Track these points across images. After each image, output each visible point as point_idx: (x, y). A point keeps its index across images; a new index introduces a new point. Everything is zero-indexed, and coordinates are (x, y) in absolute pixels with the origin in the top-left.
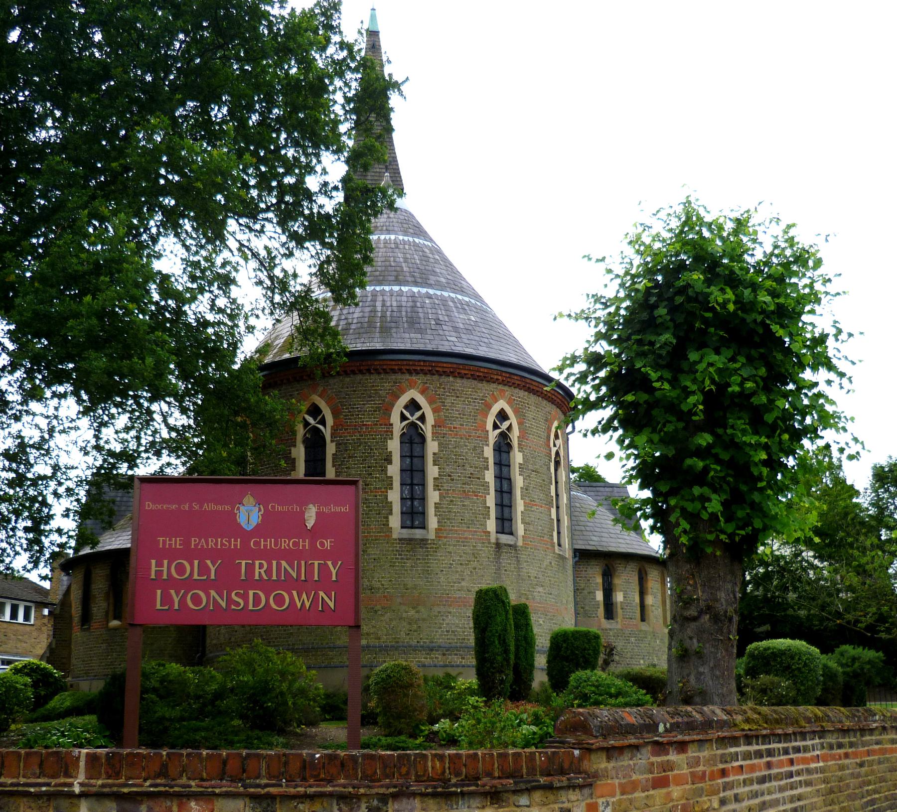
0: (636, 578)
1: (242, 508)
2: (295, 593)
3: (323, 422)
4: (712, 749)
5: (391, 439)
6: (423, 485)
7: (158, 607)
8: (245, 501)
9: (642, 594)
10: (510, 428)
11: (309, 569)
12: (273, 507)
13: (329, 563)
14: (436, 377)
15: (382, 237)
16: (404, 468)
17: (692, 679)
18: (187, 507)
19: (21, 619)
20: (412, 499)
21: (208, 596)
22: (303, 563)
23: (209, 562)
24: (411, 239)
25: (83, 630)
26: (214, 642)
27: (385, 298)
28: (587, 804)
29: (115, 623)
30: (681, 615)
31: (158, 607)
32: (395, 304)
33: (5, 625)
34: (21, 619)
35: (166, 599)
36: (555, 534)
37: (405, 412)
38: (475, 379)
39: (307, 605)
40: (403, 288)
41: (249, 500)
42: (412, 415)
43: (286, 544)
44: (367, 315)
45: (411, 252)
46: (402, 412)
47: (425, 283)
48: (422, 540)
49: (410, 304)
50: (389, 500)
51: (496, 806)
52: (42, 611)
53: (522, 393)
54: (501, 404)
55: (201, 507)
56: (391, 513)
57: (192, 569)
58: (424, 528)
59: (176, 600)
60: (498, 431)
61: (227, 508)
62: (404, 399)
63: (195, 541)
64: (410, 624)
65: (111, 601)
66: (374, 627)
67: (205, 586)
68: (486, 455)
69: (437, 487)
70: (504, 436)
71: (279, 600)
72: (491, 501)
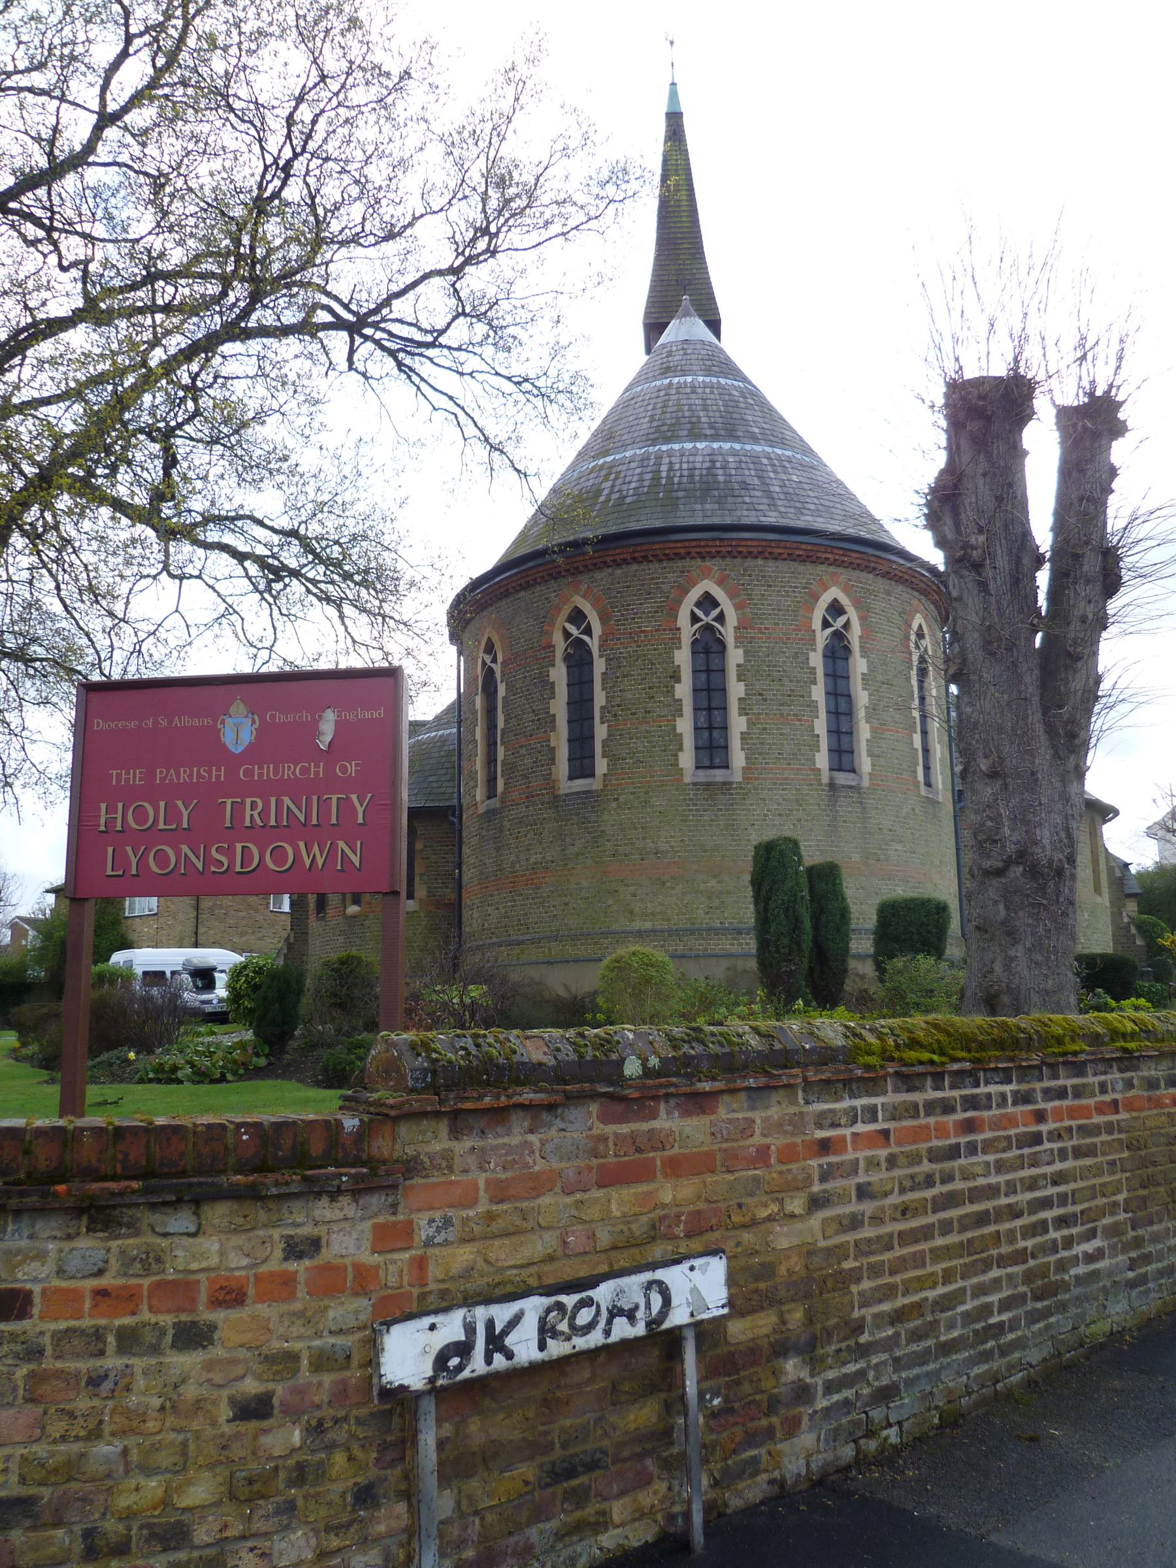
1: (228, 721)
3: (588, 631)
4: (794, 1102)
5: (679, 648)
6: (724, 709)
8: (232, 710)
10: (846, 626)
11: (324, 804)
12: (273, 717)
13: (354, 797)
14: (739, 560)
15: (676, 380)
16: (699, 686)
17: (998, 967)
18: (150, 723)
20: (710, 728)
21: (178, 853)
23: (180, 803)
24: (714, 380)
27: (674, 460)
28: (375, 1226)
29: (353, 909)
30: (980, 868)
31: (109, 872)
32: (685, 466)
35: (120, 859)
37: (697, 611)
39: (320, 861)
40: (698, 445)
41: (238, 708)
42: (707, 615)
43: (291, 771)
44: (646, 483)
46: (692, 613)
47: (732, 436)
48: (725, 783)
49: (707, 465)
50: (679, 730)
51: (101, 1235)
54: (834, 593)
55: (170, 723)
56: (681, 749)
58: (727, 767)
59: (134, 861)
60: (829, 630)
61: (207, 721)
62: (695, 594)
64: (710, 898)
66: (661, 904)
67: (175, 837)
68: (812, 664)
69: (743, 711)
70: (838, 636)
72: (821, 726)
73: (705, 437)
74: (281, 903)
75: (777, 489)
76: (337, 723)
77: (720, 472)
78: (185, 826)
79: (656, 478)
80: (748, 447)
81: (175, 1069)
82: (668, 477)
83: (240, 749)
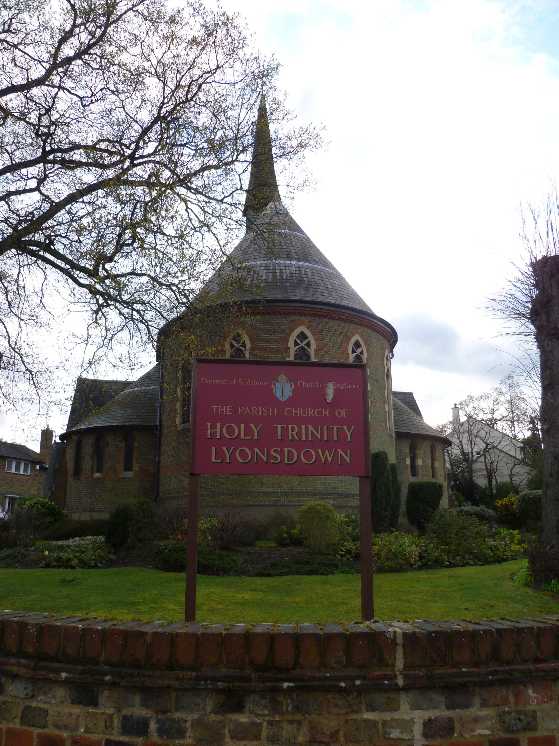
0: (429, 450)
1: (277, 384)
2: (320, 451)
3: (244, 345)
7: (214, 460)
8: (279, 379)
9: (433, 459)
10: (362, 353)
12: (301, 384)
13: (345, 428)
14: (317, 318)
19: (22, 472)
21: (253, 452)
22: (325, 427)
23: (252, 426)
25: (75, 479)
26: (166, 488)
29: (97, 475)
31: (214, 460)
32: (288, 271)
33: (12, 475)
34: (22, 472)
36: (388, 421)
38: (341, 321)
39: (330, 460)
40: (292, 262)
41: (282, 378)
43: (312, 412)
44: (271, 277)
45: (294, 240)
46: (295, 340)
47: (306, 260)
49: (298, 272)
52: (35, 467)
53: (369, 331)
54: (356, 337)
57: (239, 430)
59: (228, 456)
60: (355, 354)
62: (297, 332)
63: (241, 409)
65: (95, 460)
66: (277, 479)
67: (251, 444)
71: (308, 456)
73: (295, 259)
74: (11, 468)
75: (330, 287)
76: (335, 389)
77: (304, 276)
78: (256, 437)
79: (275, 275)
80: (315, 266)
81: (69, 560)
82: (280, 276)
83: (285, 399)
